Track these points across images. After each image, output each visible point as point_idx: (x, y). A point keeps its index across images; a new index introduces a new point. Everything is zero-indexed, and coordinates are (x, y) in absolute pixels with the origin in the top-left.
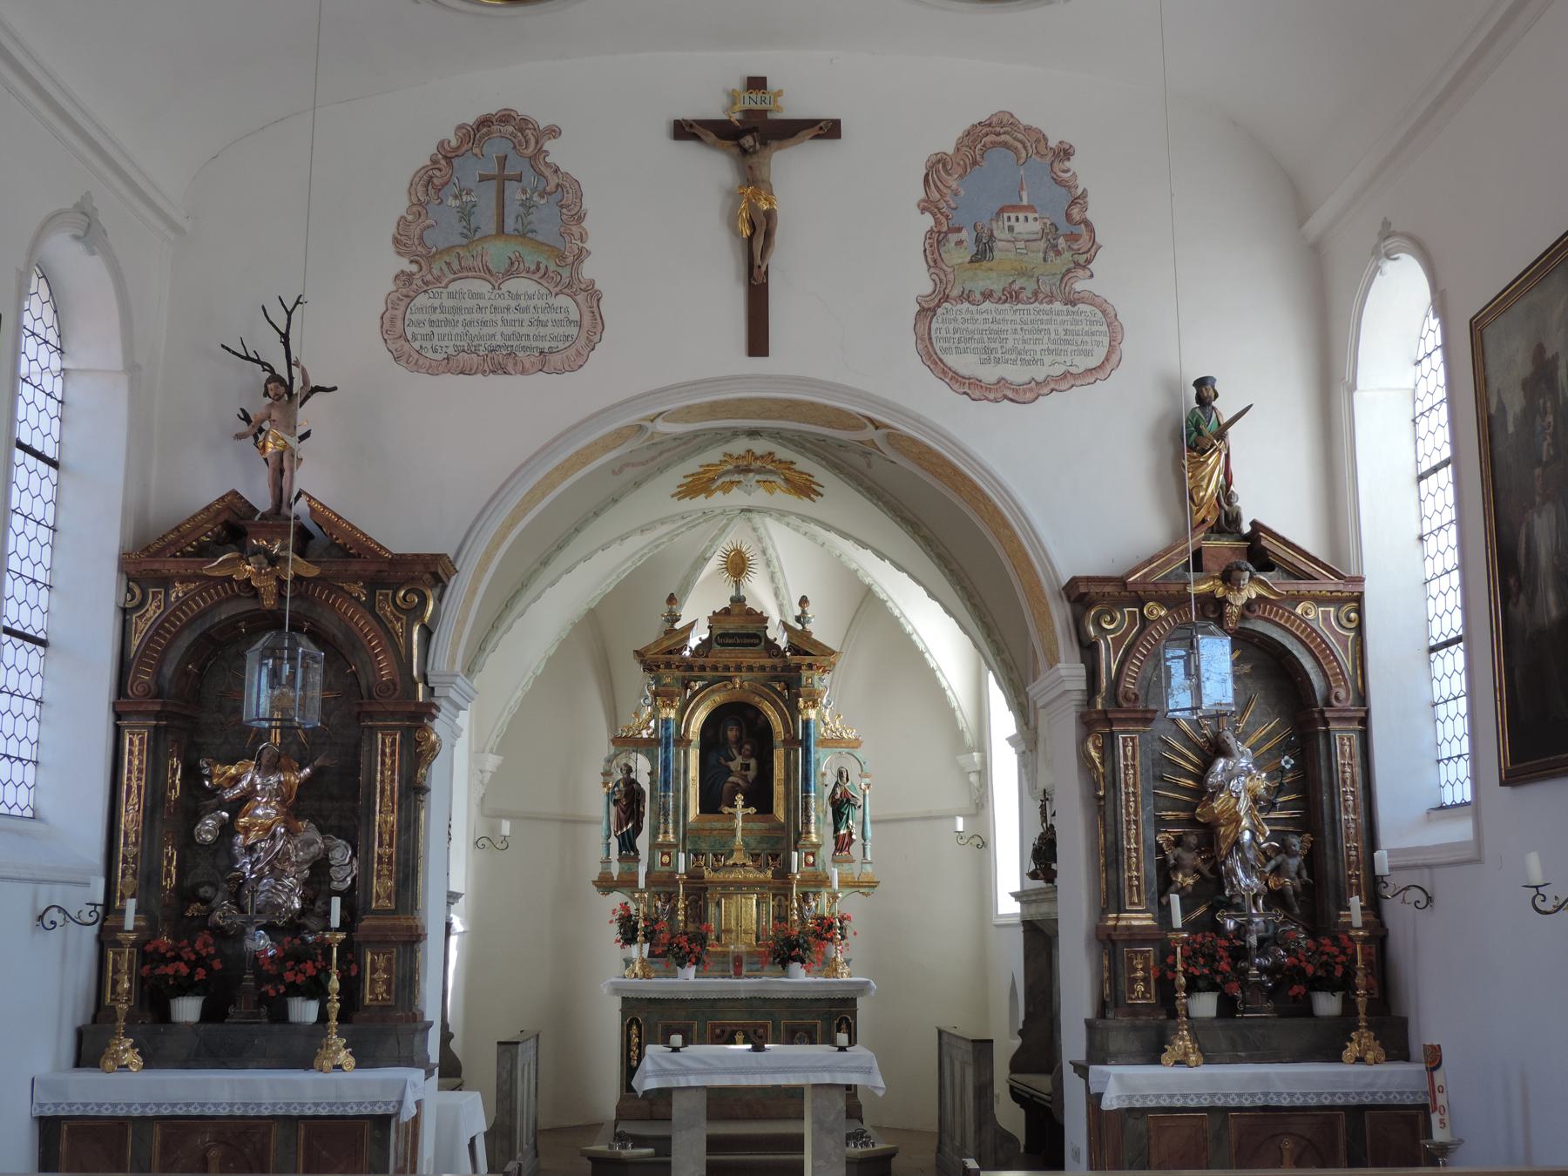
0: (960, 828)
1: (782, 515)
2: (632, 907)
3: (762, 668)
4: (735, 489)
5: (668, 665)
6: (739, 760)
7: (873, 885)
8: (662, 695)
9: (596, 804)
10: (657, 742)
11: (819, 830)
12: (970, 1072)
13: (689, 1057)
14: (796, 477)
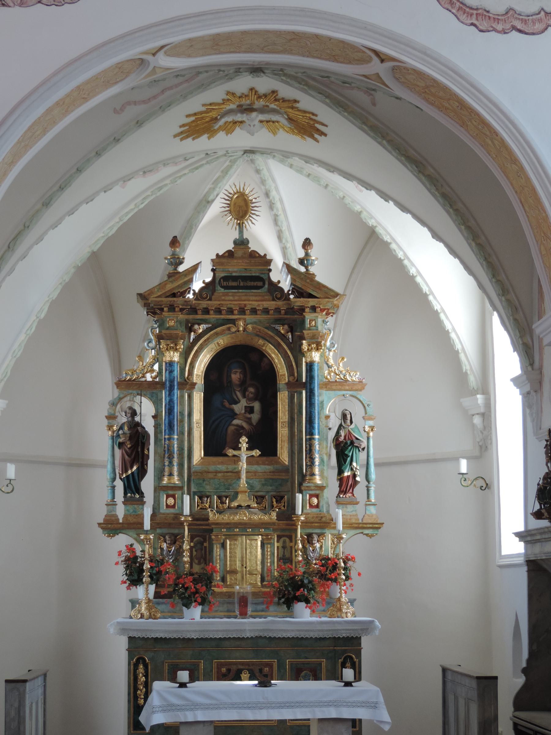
0: (464, 470)
1: (285, 156)
2: (138, 549)
3: (266, 311)
4: (238, 131)
5: (172, 308)
6: (243, 403)
7: (377, 526)
8: (166, 338)
9: (101, 448)
10: (162, 385)
11: (324, 471)
12: (474, 709)
13: (195, 692)
14: (299, 117)
